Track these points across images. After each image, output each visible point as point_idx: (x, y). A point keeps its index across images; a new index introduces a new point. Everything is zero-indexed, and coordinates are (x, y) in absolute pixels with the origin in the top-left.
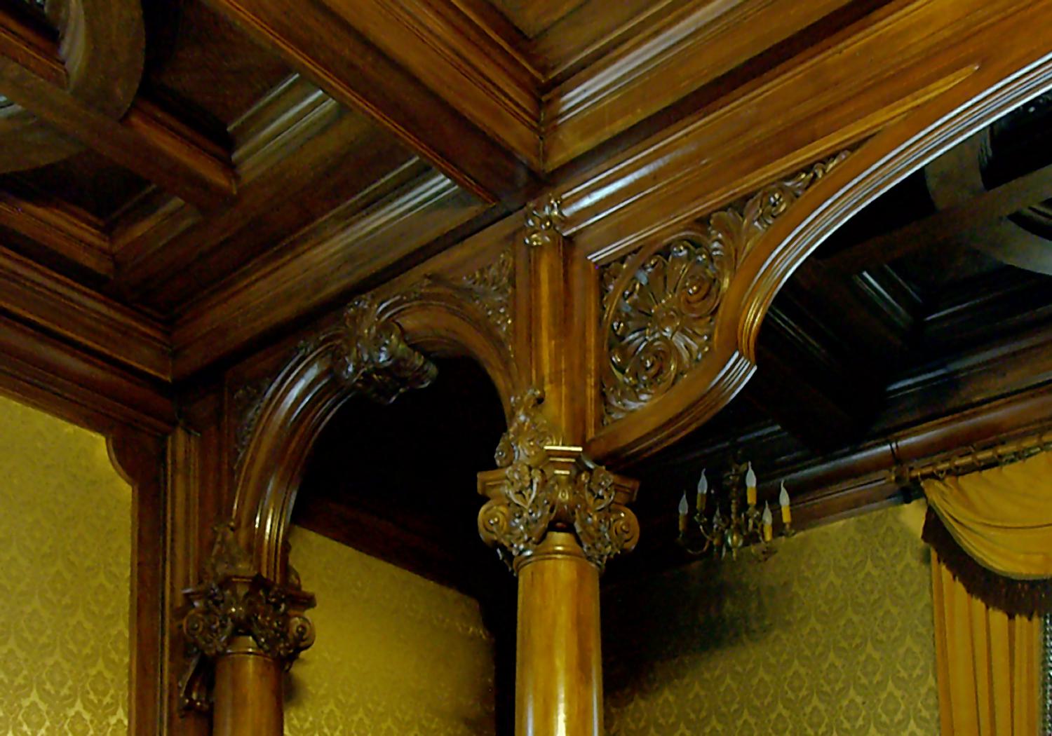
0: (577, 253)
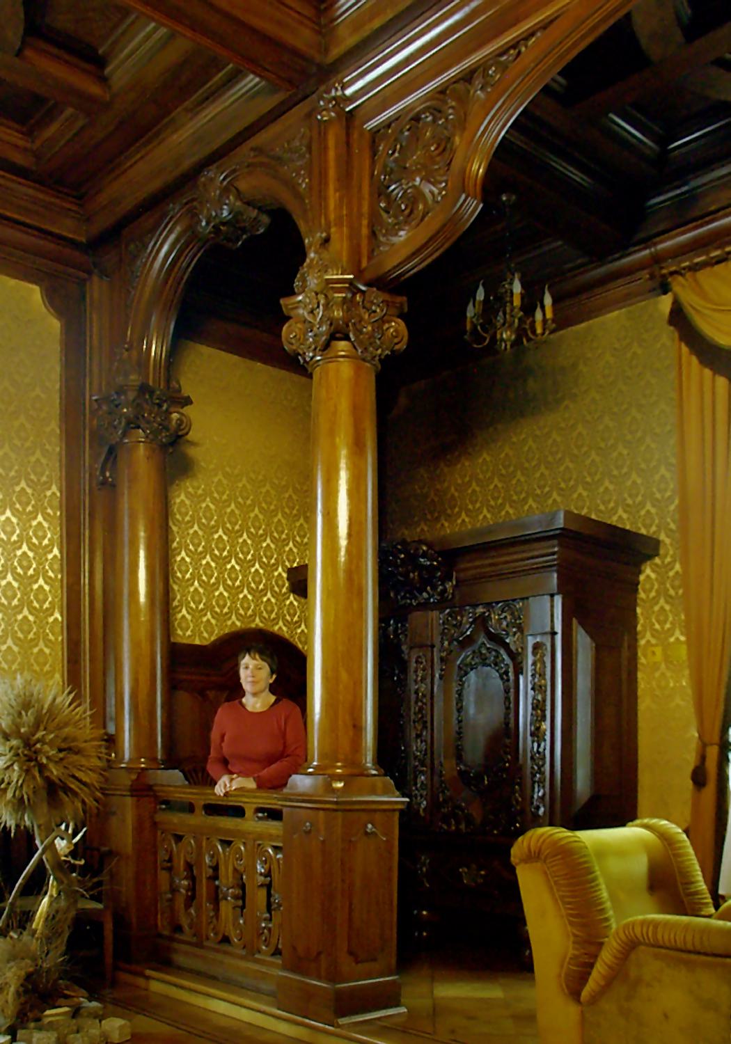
0: (357, 123)
